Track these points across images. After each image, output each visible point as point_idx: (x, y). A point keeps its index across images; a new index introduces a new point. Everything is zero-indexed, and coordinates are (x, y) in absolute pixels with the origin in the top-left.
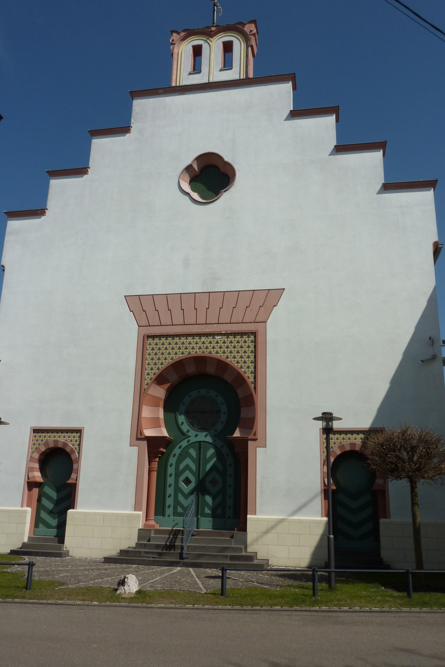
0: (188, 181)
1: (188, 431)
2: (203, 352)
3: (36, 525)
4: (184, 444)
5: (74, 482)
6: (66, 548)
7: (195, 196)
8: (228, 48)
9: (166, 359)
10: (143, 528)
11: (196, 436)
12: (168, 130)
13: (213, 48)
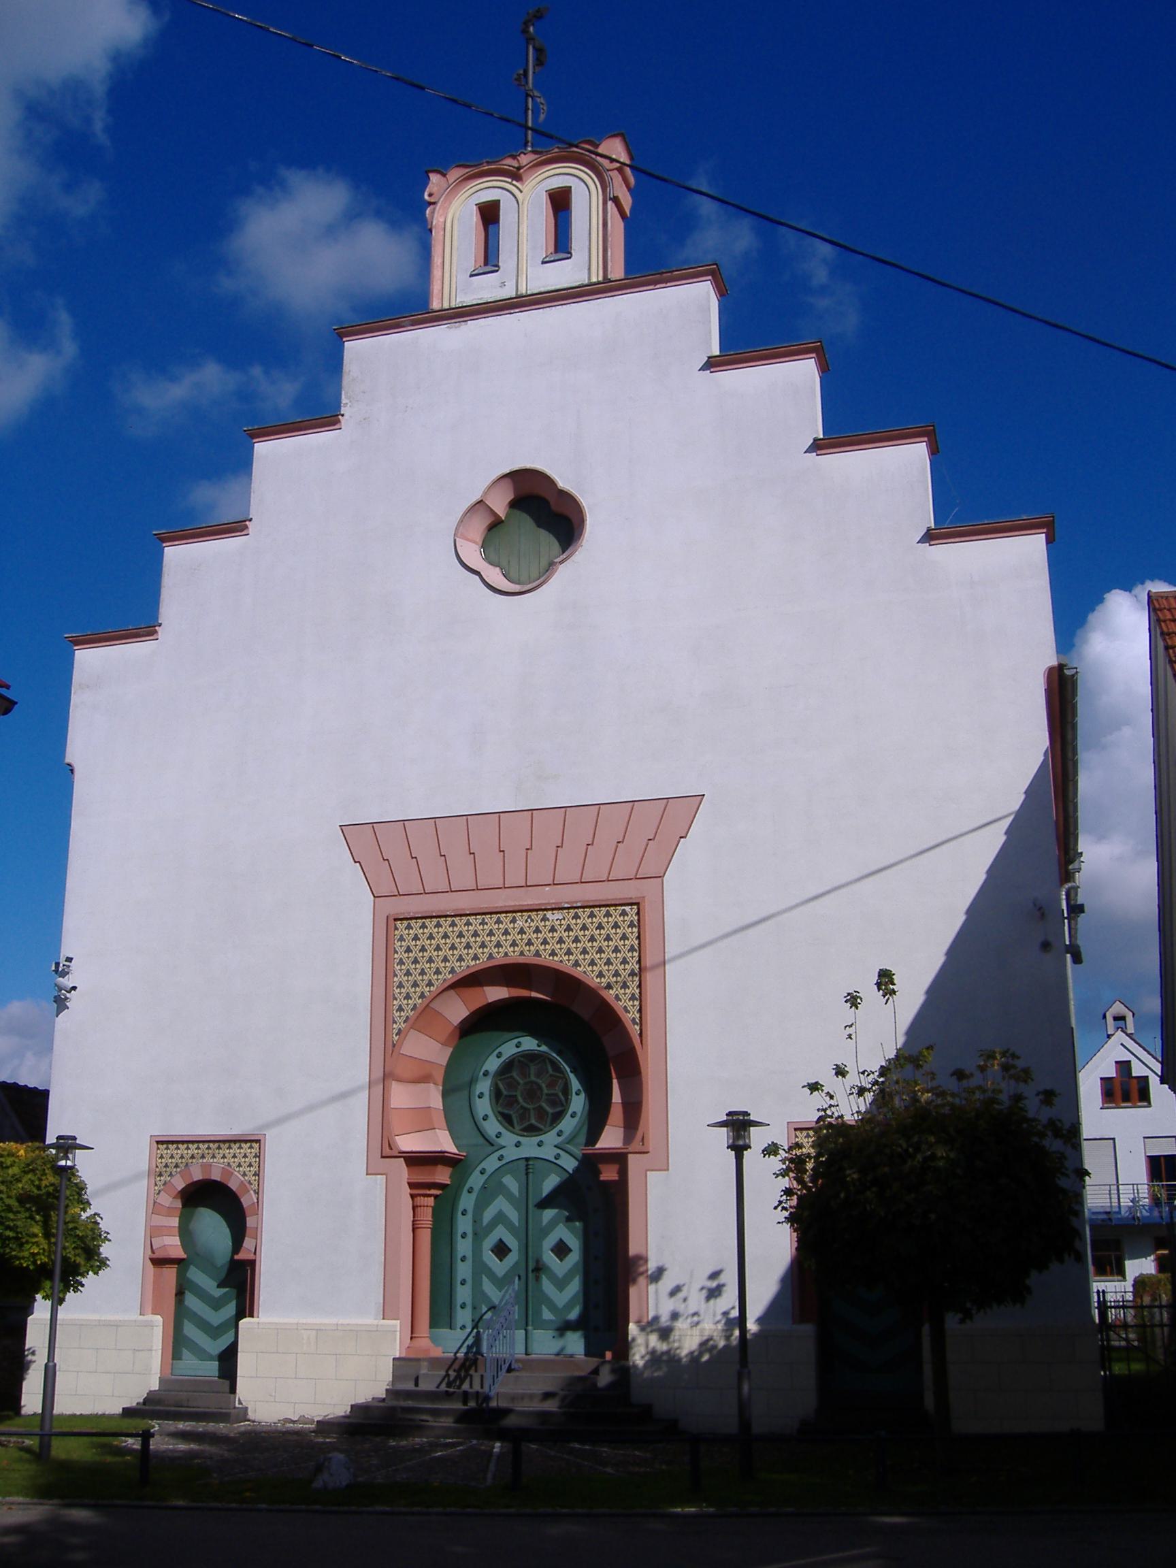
0: (479, 539)
1: (499, 1135)
2: (522, 953)
3: (176, 1355)
4: (491, 1164)
5: (251, 1257)
6: (240, 1403)
7: (494, 575)
8: (560, 201)
9: (438, 972)
10: (403, 1355)
11: (518, 1145)
12: (433, 408)
13: (526, 202)
